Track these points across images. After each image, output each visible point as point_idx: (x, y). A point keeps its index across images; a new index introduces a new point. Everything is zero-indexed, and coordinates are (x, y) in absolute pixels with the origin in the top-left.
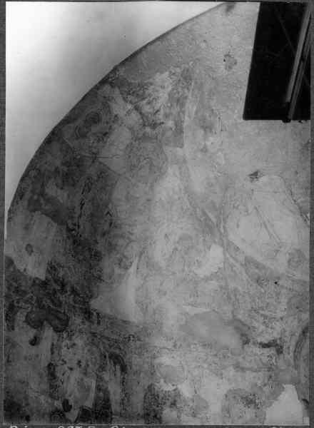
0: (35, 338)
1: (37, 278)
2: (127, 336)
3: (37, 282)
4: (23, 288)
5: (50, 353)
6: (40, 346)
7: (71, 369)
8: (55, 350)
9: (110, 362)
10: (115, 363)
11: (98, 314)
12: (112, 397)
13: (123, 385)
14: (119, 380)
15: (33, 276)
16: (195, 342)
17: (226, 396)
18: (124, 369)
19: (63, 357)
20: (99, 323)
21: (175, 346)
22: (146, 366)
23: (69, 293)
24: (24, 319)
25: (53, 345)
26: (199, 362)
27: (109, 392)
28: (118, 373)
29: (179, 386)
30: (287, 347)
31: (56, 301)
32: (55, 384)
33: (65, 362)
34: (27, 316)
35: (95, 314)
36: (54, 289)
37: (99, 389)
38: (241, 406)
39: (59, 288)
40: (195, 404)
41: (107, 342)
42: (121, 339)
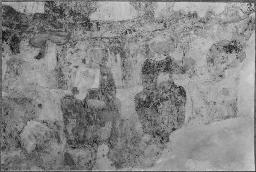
0: (40, 54)
1: (37, 13)
2: (124, 31)
3: (38, 16)
4: (24, 24)
5: (55, 60)
6: (46, 57)
7: (77, 67)
8: (59, 57)
9: (111, 54)
10: (115, 53)
11: (97, 24)
12: (115, 77)
13: (123, 67)
14: (120, 64)
15: (33, 13)
16: (34, 162)
17: (210, 50)
18: (123, 55)
19: (68, 61)
20: (99, 29)
21: (165, 26)
22: (107, 83)
23: (68, 16)
24: (28, 44)
25: (57, 55)
26: (186, 31)
27: (111, 75)
28: (119, 59)
29: (170, 55)
30: (91, 149)
31: (57, 25)
32: (64, 79)
33: (71, 64)
34: (30, 42)
35: (94, 24)
36: (54, 17)
37: (103, 74)
38: (224, 54)
39: (58, 15)
40: (184, 64)
41: (107, 41)
42: (119, 35)
